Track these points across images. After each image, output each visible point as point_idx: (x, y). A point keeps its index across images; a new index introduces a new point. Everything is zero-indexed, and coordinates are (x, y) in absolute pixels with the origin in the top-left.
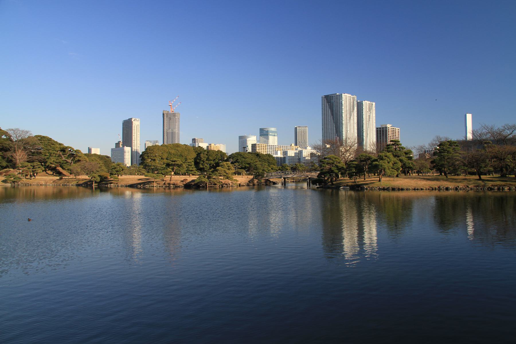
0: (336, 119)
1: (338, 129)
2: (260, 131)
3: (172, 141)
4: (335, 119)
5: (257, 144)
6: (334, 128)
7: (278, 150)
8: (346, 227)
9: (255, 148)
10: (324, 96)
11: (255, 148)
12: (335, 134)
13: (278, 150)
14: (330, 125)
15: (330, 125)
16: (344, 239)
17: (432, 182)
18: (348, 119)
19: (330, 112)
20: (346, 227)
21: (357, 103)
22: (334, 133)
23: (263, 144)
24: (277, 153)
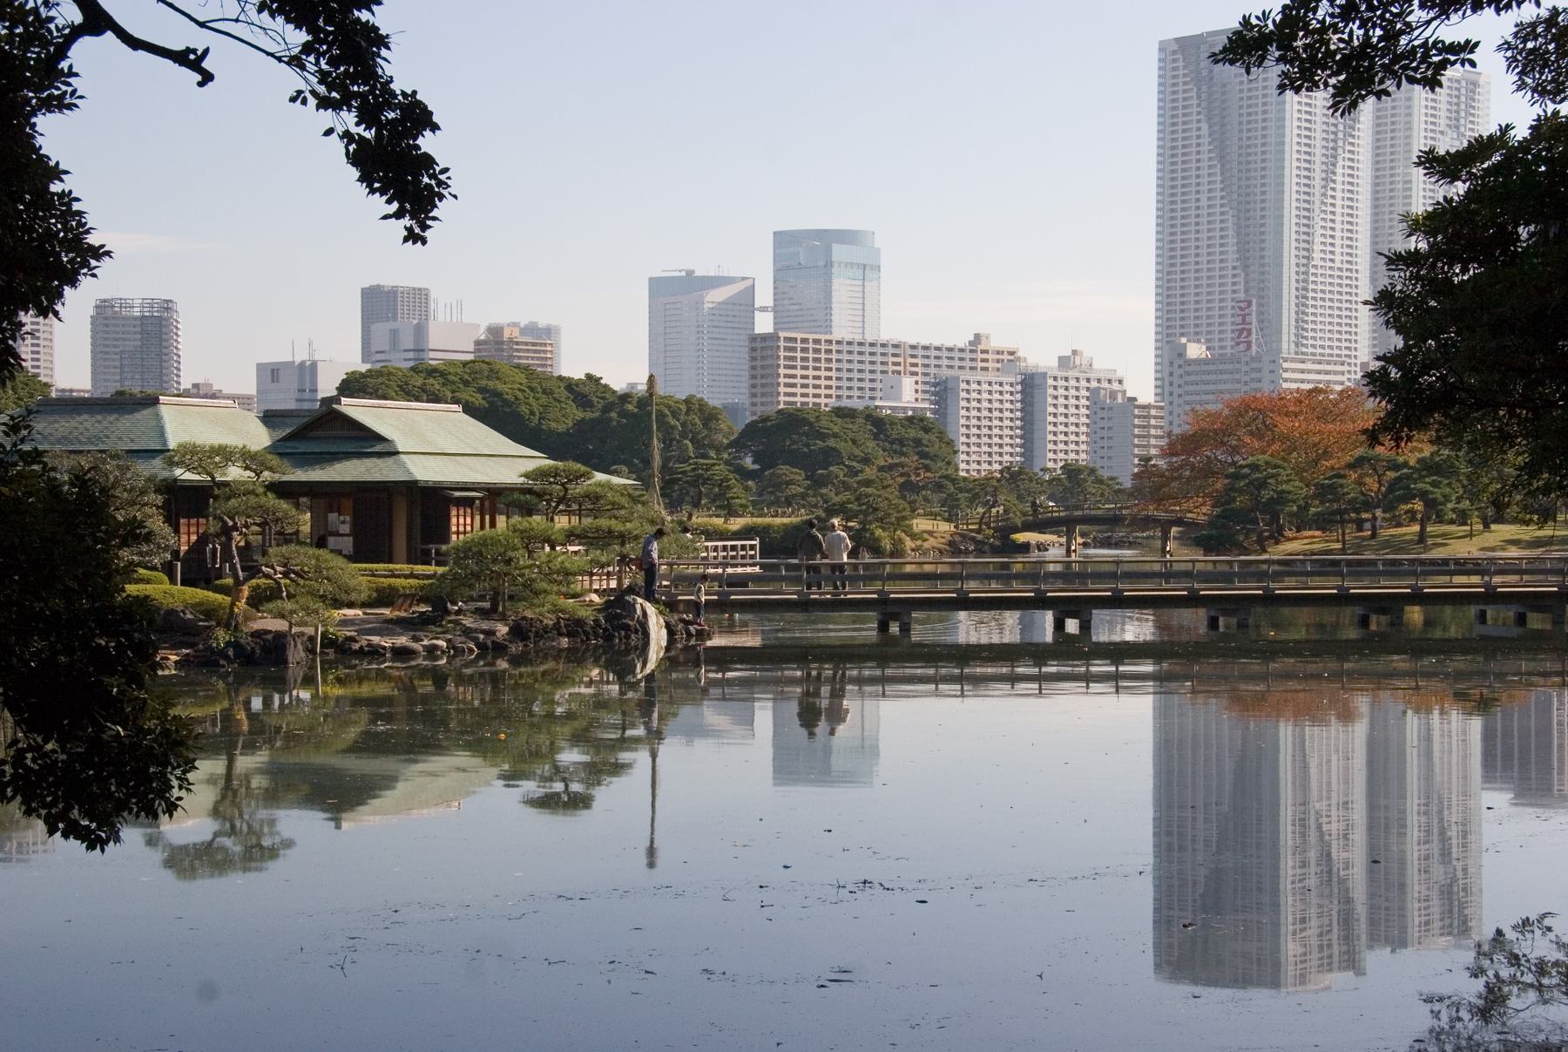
0: (1244, 183)
1: (1252, 166)
2: (775, 248)
3: (873, 630)
4: (1235, 180)
5: (782, 334)
6: (1232, 240)
7: (901, 368)
8: (1440, 423)
9: (769, 362)
10: (1177, 40)
11: (772, 356)
12: (1234, 276)
13: (901, 368)
14: (1204, 235)
15: (1205, 180)
16: (1481, 136)
17: (1364, 802)
18: (1318, 175)
19: (1206, 140)
20: (1440, 423)
21: (1378, 148)
22: (1230, 264)
23: (817, 337)
24: (895, 391)
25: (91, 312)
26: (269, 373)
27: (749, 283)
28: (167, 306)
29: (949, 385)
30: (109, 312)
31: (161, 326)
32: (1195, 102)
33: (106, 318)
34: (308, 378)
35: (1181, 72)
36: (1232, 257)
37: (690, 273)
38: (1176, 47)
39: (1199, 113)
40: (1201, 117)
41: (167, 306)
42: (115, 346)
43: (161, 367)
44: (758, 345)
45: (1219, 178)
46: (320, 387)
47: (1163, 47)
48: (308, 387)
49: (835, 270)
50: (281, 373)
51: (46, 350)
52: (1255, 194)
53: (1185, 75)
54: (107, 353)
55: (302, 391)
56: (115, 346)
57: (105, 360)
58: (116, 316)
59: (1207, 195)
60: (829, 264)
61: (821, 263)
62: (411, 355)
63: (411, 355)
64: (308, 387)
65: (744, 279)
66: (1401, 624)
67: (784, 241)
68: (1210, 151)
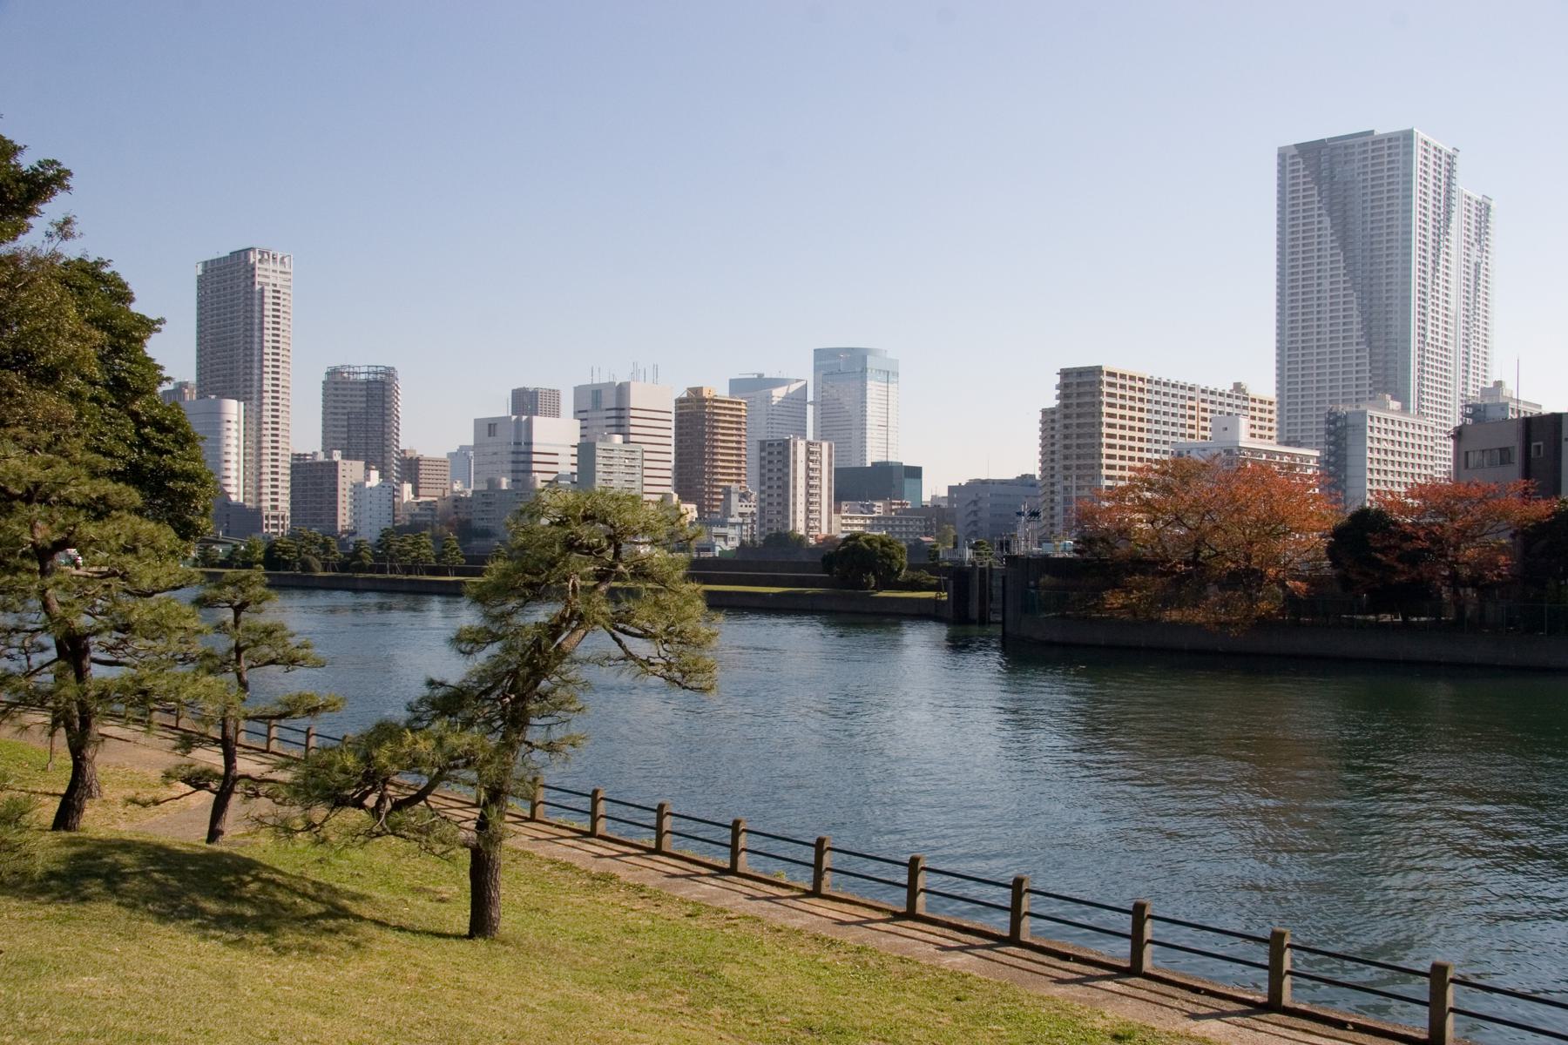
22: (1355, 340)
25: (323, 377)
26: (487, 428)
27: (803, 383)
28: (390, 373)
29: (1350, 421)
30: (338, 378)
31: (384, 389)
32: (1316, 198)
33: (336, 383)
34: (524, 432)
35: (1301, 173)
36: (1356, 333)
37: (760, 376)
38: (1296, 152)
39: (1319, 208)
40: (1323, 212)
41: (390, 373)
42: (344, 408)
43: (383, 426)
44: (1074, 380)
45: (1342, 265)
46: (535, 440)
47: (1282, 155)
48: (523, 440)
49: (869, 374)
50: (498, 427)
51: (284, 402)
52: (1380, 278)
53: (1304, 176)
54: (336, 414)
55: (518, 444)
56: (344, 408)
57: (335, 420)
58: (346, 382)
59: (1329, 280)
60: (864, 370)
61: (859, 369)
62: (613, 413)
63: (613, 413)
64: (523, 440)
65: (798, 381)
66: (171, 522)
67: (823, 357)
68: (1332, 241)
